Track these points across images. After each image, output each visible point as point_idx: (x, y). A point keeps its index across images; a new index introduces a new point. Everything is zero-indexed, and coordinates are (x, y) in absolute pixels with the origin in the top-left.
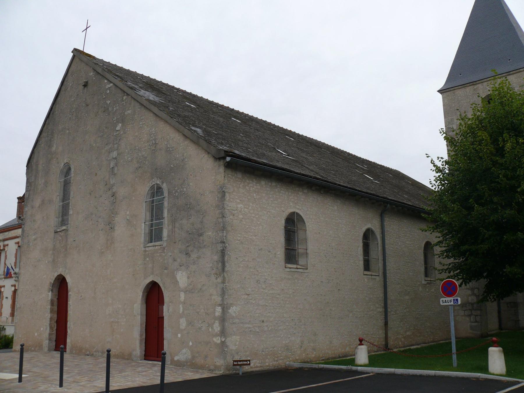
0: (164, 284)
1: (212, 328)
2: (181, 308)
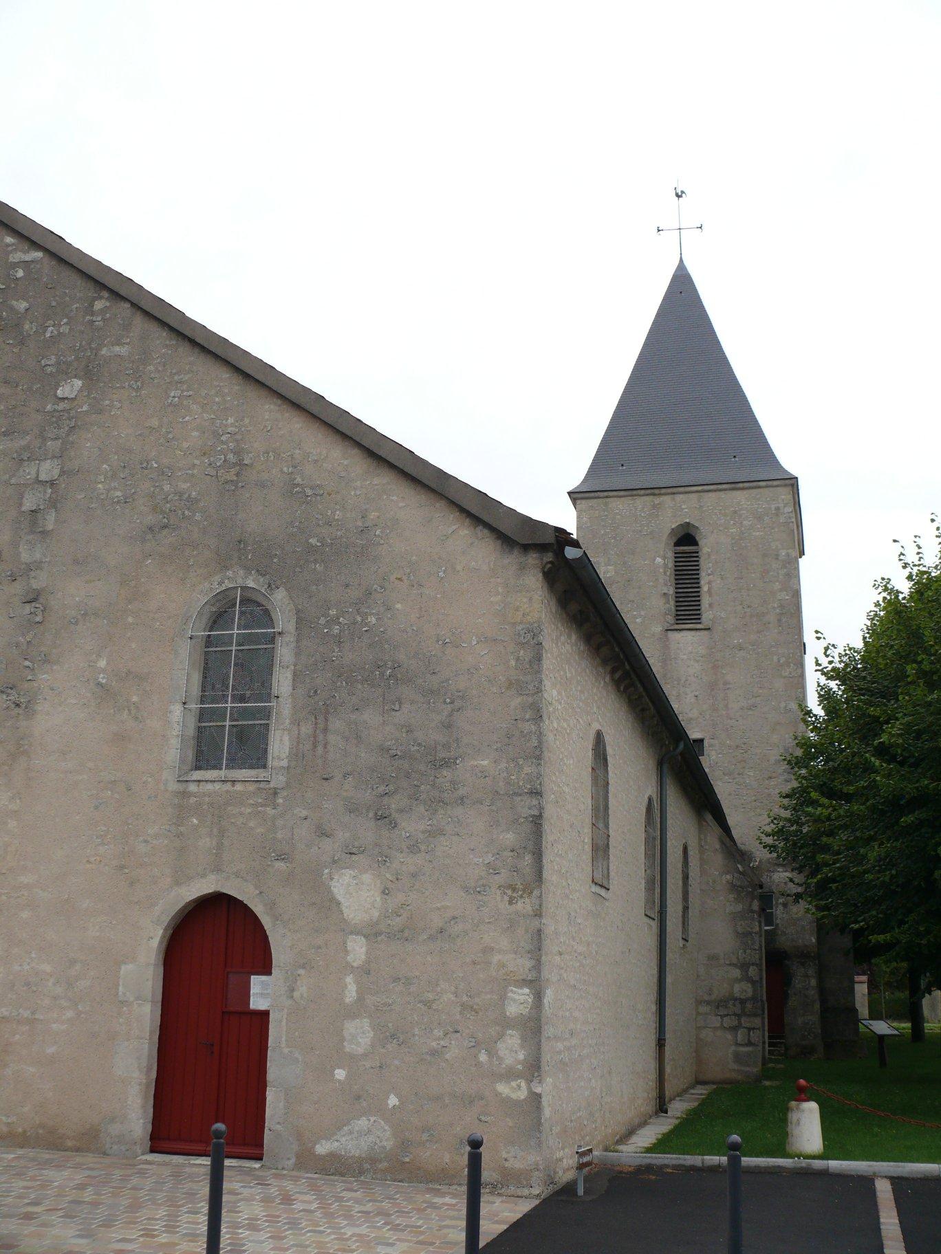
0: (271, 906)
1: (491, 1053)
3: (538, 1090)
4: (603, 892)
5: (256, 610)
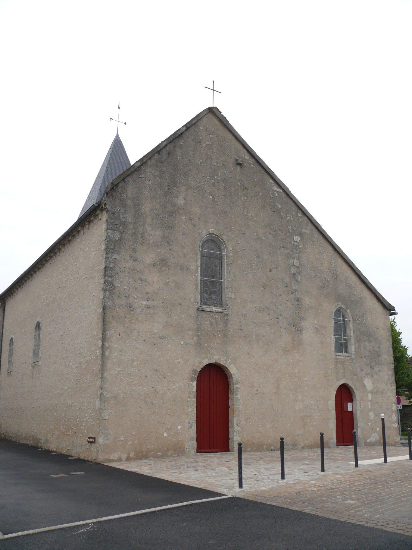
0: (355, 387)
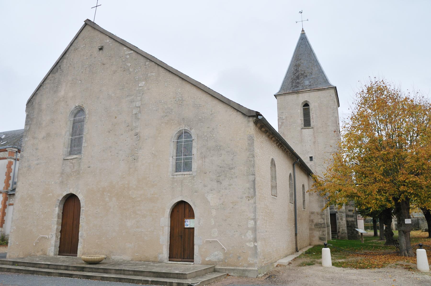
0: (194, 203)
2: (213, 221)
3: (256, 244)
4: (275, 197)
5: (187, 134)
